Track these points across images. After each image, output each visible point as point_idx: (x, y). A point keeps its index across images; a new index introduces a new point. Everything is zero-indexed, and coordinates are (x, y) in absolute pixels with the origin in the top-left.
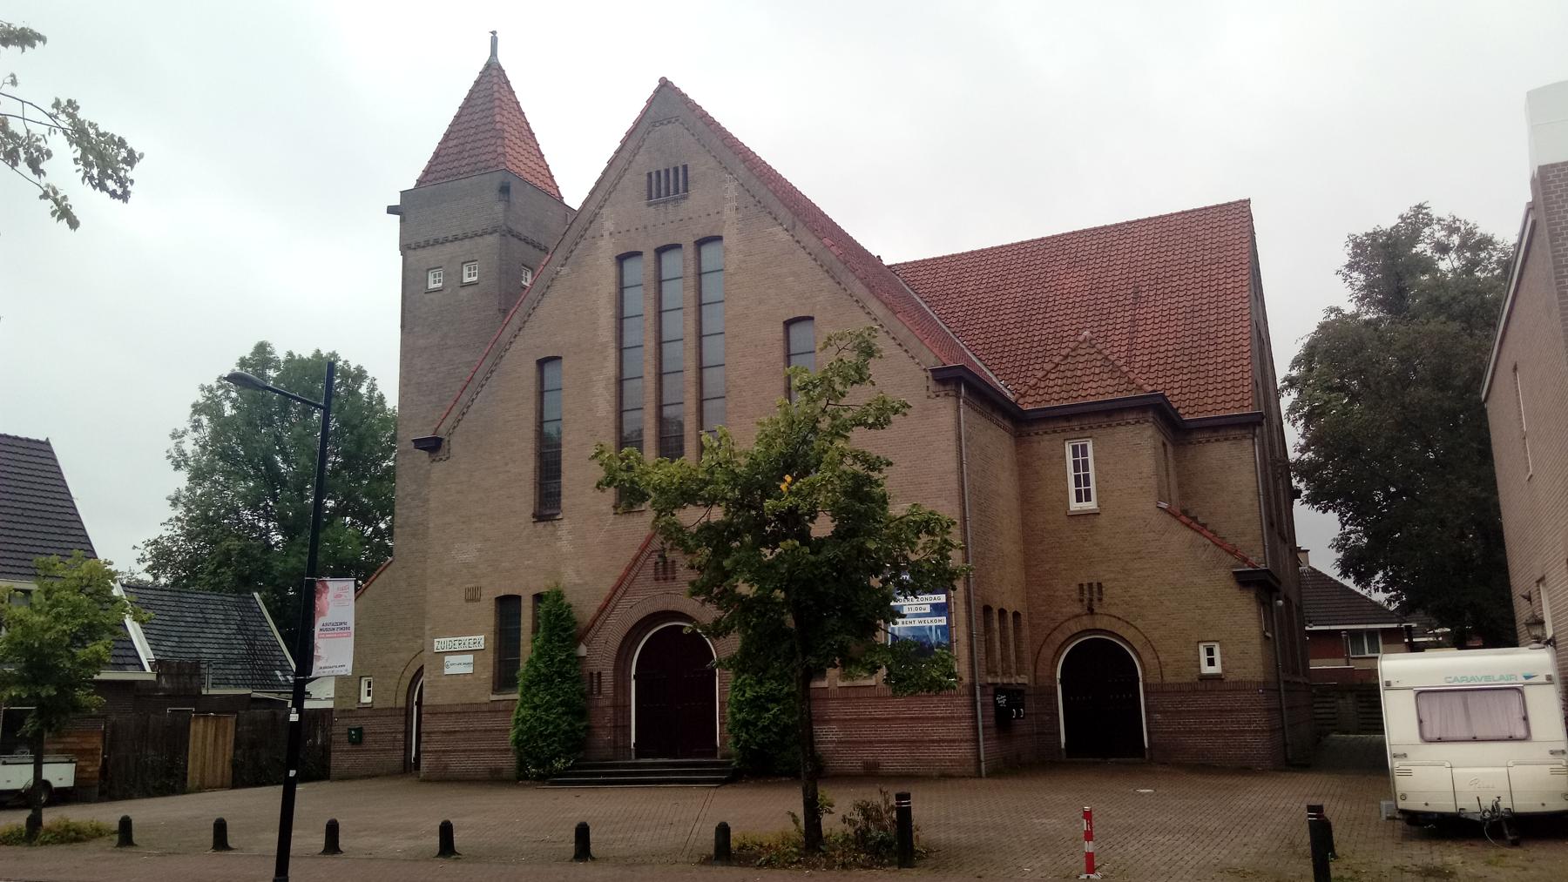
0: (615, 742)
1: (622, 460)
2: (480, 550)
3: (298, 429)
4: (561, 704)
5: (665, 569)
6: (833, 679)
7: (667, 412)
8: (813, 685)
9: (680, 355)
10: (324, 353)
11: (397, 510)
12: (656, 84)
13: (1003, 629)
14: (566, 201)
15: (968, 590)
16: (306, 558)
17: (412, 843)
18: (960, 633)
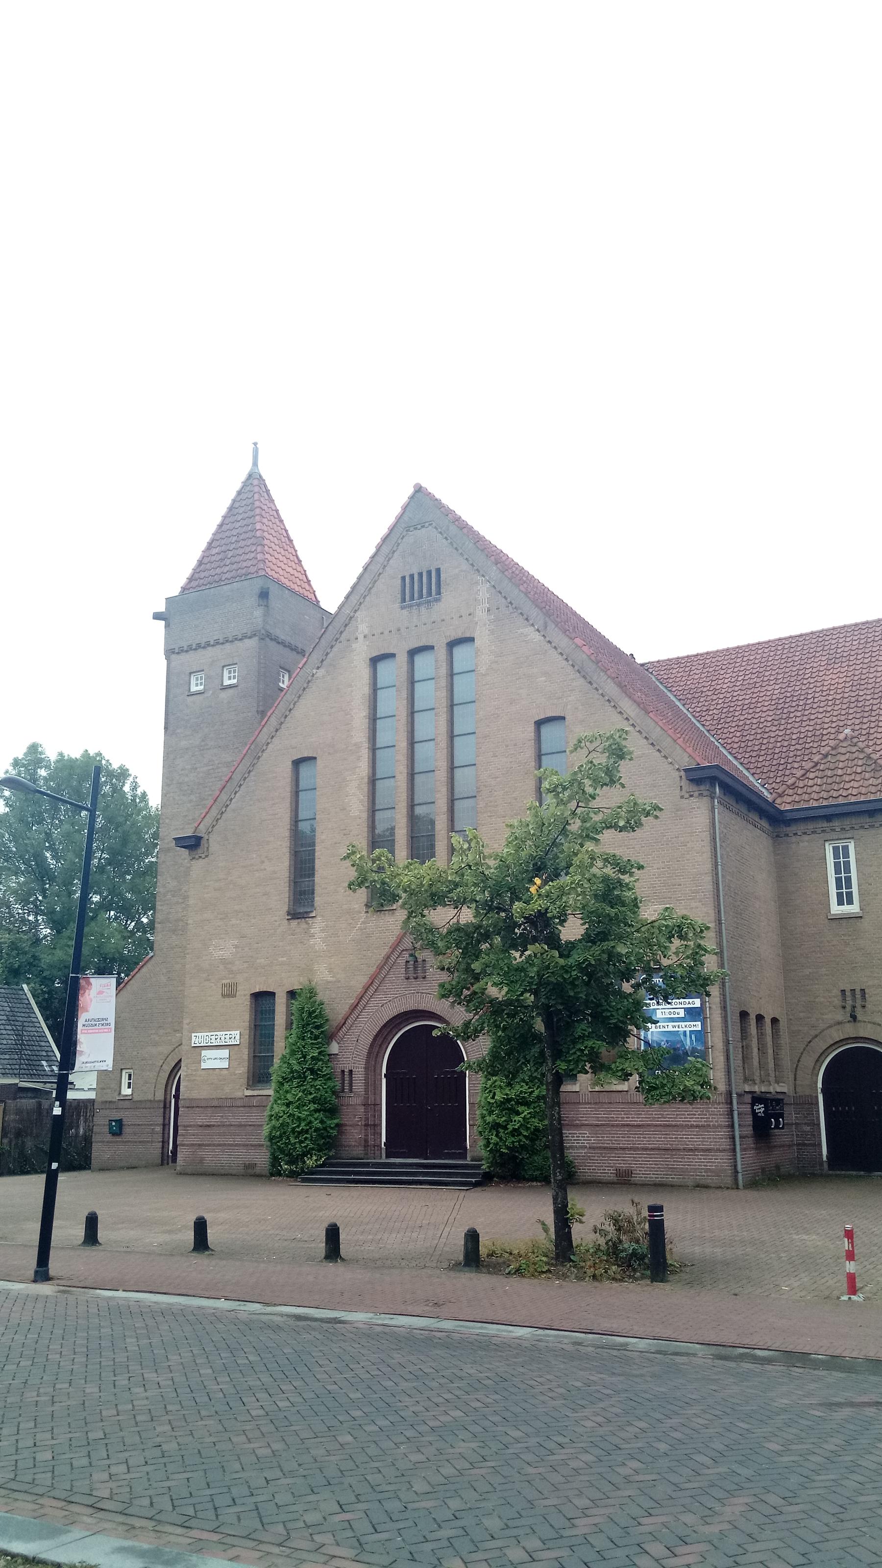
0: (366, 1141)
1: (374, 861)
2: (236, 947)
3: (66, 827)
4: (314, 1101)
5: (415, 968)
6: (582, 1085)
7: (418, 810)
8: (563, 1088)
9: (431, 755)
10: (92, 753)
11: (158, 907)
12: (411, 491)
13: (761, 1035)
14: (323, 605)
15: (723, 995)
16: (71, 951)
17: (166, 1238)
18: (716, 1039)
